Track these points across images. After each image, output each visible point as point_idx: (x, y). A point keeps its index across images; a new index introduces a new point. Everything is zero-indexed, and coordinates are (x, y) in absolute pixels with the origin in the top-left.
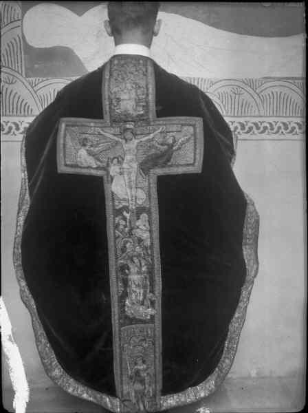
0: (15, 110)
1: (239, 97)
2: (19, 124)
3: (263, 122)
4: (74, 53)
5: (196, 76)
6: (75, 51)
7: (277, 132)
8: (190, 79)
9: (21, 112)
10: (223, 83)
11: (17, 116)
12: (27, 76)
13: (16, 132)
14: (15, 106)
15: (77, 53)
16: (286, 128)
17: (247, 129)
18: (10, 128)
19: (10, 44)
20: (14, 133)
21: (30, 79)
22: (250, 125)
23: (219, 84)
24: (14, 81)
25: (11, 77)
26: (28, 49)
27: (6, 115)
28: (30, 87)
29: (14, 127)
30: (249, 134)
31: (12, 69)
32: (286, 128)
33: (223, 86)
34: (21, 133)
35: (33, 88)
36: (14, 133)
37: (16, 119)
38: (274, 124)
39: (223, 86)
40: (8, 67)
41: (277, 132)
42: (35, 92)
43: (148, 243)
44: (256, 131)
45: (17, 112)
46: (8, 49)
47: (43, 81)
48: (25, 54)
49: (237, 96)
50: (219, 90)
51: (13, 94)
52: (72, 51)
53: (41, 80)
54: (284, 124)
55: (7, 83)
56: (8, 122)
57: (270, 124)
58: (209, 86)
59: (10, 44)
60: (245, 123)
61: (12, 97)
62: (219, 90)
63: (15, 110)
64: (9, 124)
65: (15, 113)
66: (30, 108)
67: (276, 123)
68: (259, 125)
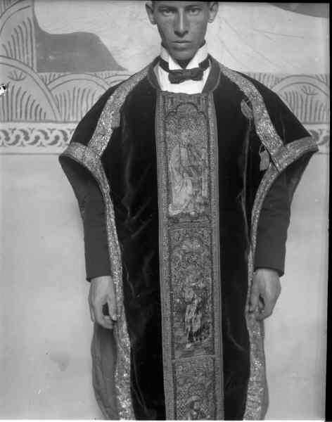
0: (23, 114)
1: (312, 98)
2: (29, 131)
3: (54, 129)
4: (100, 41)
5: (260, 71)
6: (101, 37)
7: (35, 142)
8: (249, 74)
9: (31, 117)
10: (290, 81)
11: (26, 121)
12: (39, 71)
13: (25, 143)
14: (24, 105)
15: (106, 41)
16: (27, 138)
17: (32, 139)
18: (18, 137)
19: (18, 30)
20: (22, 143)
21: (43, 74)
22: (36, 133)
23: (290, 81)
24: (23, 77)
25: (19, 73)
26: (41, 36)
27: (12, 120)
28: (42, 85)
29: (22, 136)
30: (36, 145)
31: (20, 62)
32: (27, 138)
33: (292, 84)
34: (66, 144)
35: (46, 85)
36: (22, 143)
37: (25, 126)
38: (10, 132)
39: (292, 84)
40: (15, 59)
41: (35, 142)
42: (50, 91)
43: (178, 354)
44: (45, 142)
45: (26, 116)
46: (15, 36)
47: (59, 77)
48: (37, 42)
49: (310, 96)
50: (286, 90)
51: (22, 93)
52: (98, 38)
53: (56, 77)
54: (25, 133)
55: (12, 79)
56: (15, 129)
57: (63, 132)
58: (273, 83)
59: (18, 30)
60: (319, 132)
61: (20, 97)
62: (286, 90)
63: (23, 114)
64: (16, 133)
65: (23, 118)
66: (43, 111)
67: (52, 131)
68: (49, 135)
